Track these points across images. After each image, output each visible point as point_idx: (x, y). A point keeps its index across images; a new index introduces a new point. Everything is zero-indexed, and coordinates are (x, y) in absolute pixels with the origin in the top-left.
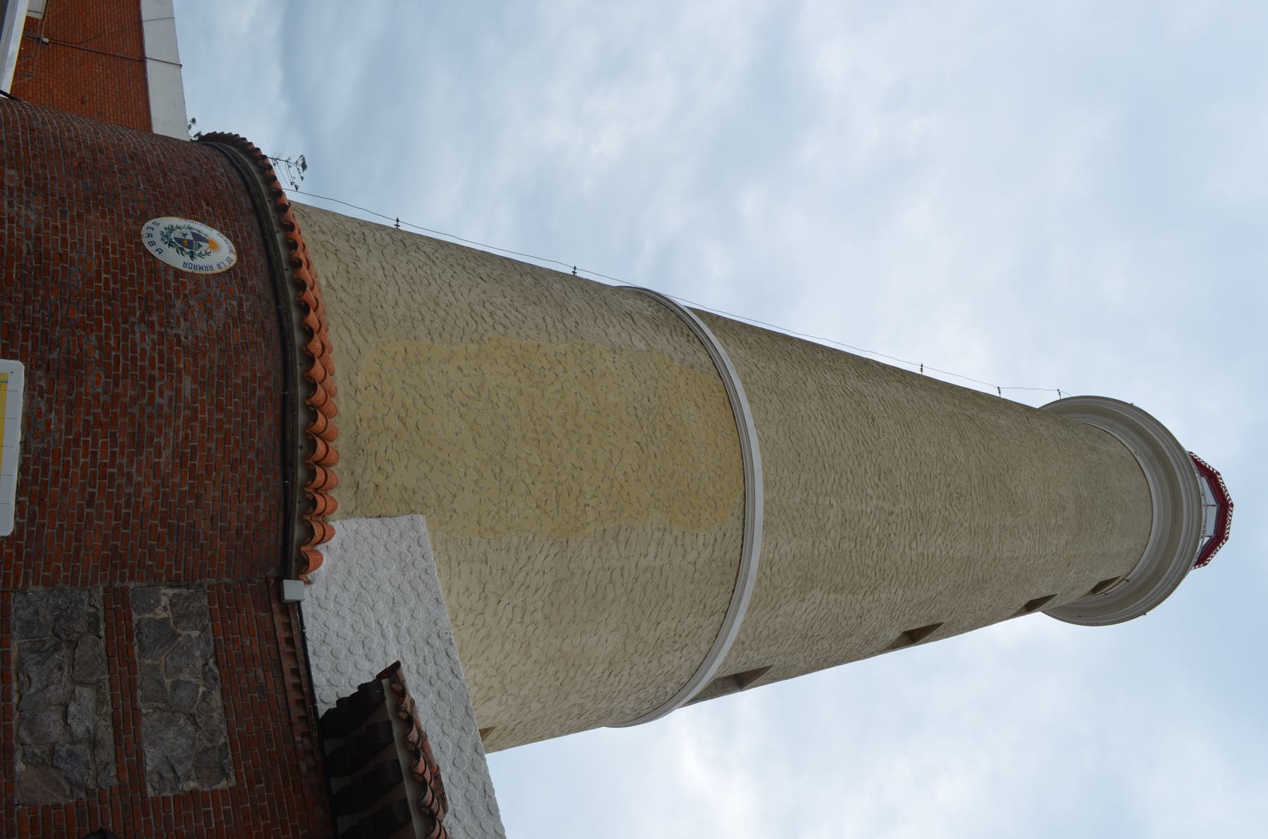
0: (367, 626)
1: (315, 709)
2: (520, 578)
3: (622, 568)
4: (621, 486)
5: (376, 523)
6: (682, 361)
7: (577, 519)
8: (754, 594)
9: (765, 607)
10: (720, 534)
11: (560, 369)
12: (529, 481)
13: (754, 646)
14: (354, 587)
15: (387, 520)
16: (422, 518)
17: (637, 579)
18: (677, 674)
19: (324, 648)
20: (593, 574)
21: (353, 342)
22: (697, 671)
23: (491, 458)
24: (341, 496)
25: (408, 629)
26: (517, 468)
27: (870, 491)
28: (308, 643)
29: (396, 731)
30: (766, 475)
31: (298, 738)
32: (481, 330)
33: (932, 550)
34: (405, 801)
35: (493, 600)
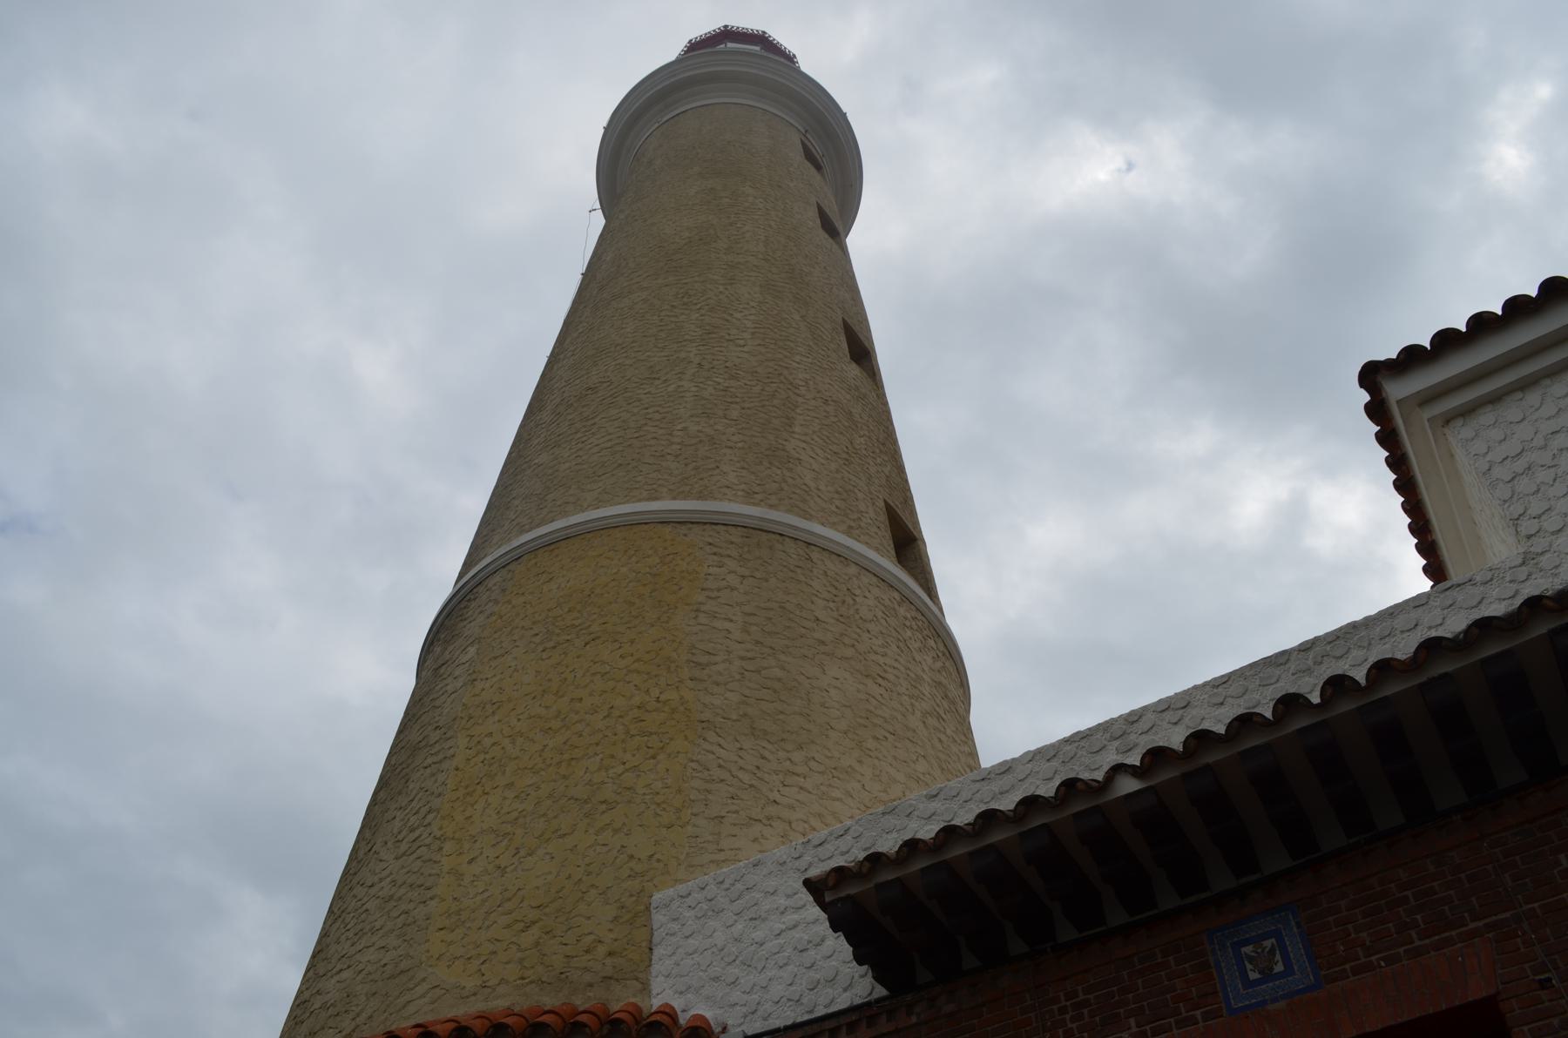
0: (781, 949)
1: (878, 1001)
2: (745, 777)
3: (742, 658)
4: (638, 660)
5: (658, 952)
6: (496, 602)
7: (674, 711)
8: (788, 511)
9: (804, 501)
10: (708, 548)
11: (487, 742)
12: (621, 769)
13: (855, 516)
14: (734, 971)
15: (656, 939)
16: (658, 897)
17: (758, 642)
18: (887, 602)
19: (805, 1001)
20: (747, 692)
21: (423, 996)
22: (906, 599)
23: (587, 815)
24: (619, 1000)
25: (788, 896)
26: (603, 783)
27: (670, 389)
28: (799, 1020)
29: (888, 876)
30: (640, 500)
31: (914, 1019)
32: (427, 841)
33: (749, 324)
34: (971, 854)
35: (772, 810)
